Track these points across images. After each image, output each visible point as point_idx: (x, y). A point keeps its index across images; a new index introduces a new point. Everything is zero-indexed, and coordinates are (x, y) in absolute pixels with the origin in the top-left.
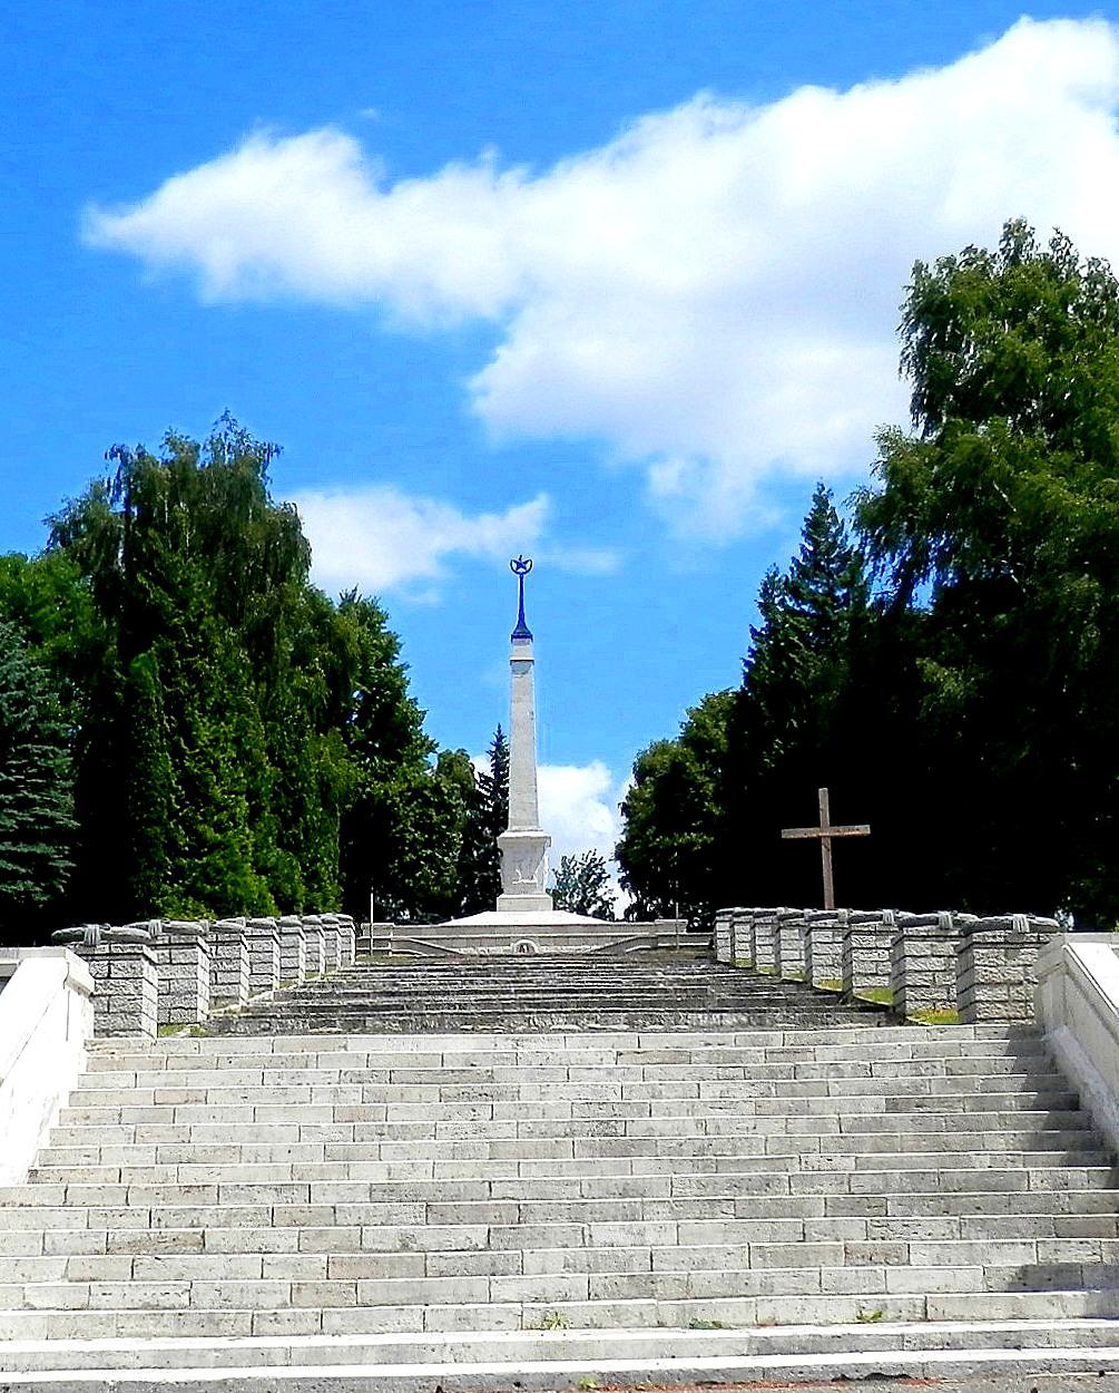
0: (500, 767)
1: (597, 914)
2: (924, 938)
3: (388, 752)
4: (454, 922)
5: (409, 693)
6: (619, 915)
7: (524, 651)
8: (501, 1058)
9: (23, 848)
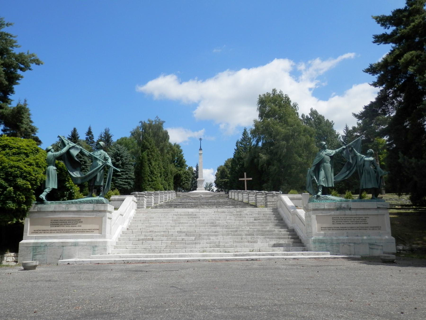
0: (197, 167)
1: (211, 191)
2: (260, 195)
4: (190, 192)
5: (184, 158)
6: (215, 191)
7: (201, 152)
8: (197, 212)
9: (126, 181)
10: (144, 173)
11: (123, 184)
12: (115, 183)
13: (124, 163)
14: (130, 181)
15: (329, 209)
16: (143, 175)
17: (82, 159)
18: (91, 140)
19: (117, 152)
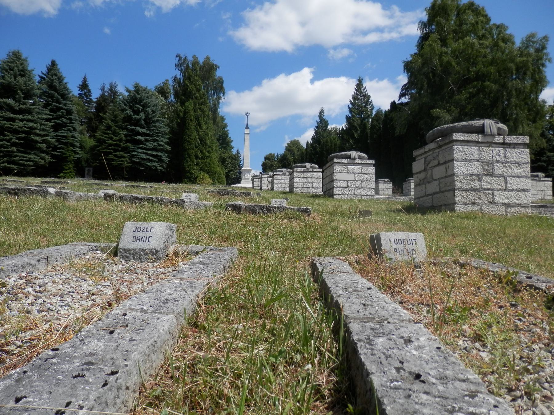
3: (225, 148)
5: (229, 136)
7: (247, 131)
9: (155, 153)
10: (189, 142)
11: (149, 159)
12: (131, 157)
13: (150, 119)
14: (162, 154)
17: (61, 106)
18: (87, 97)
19: (135, 95)
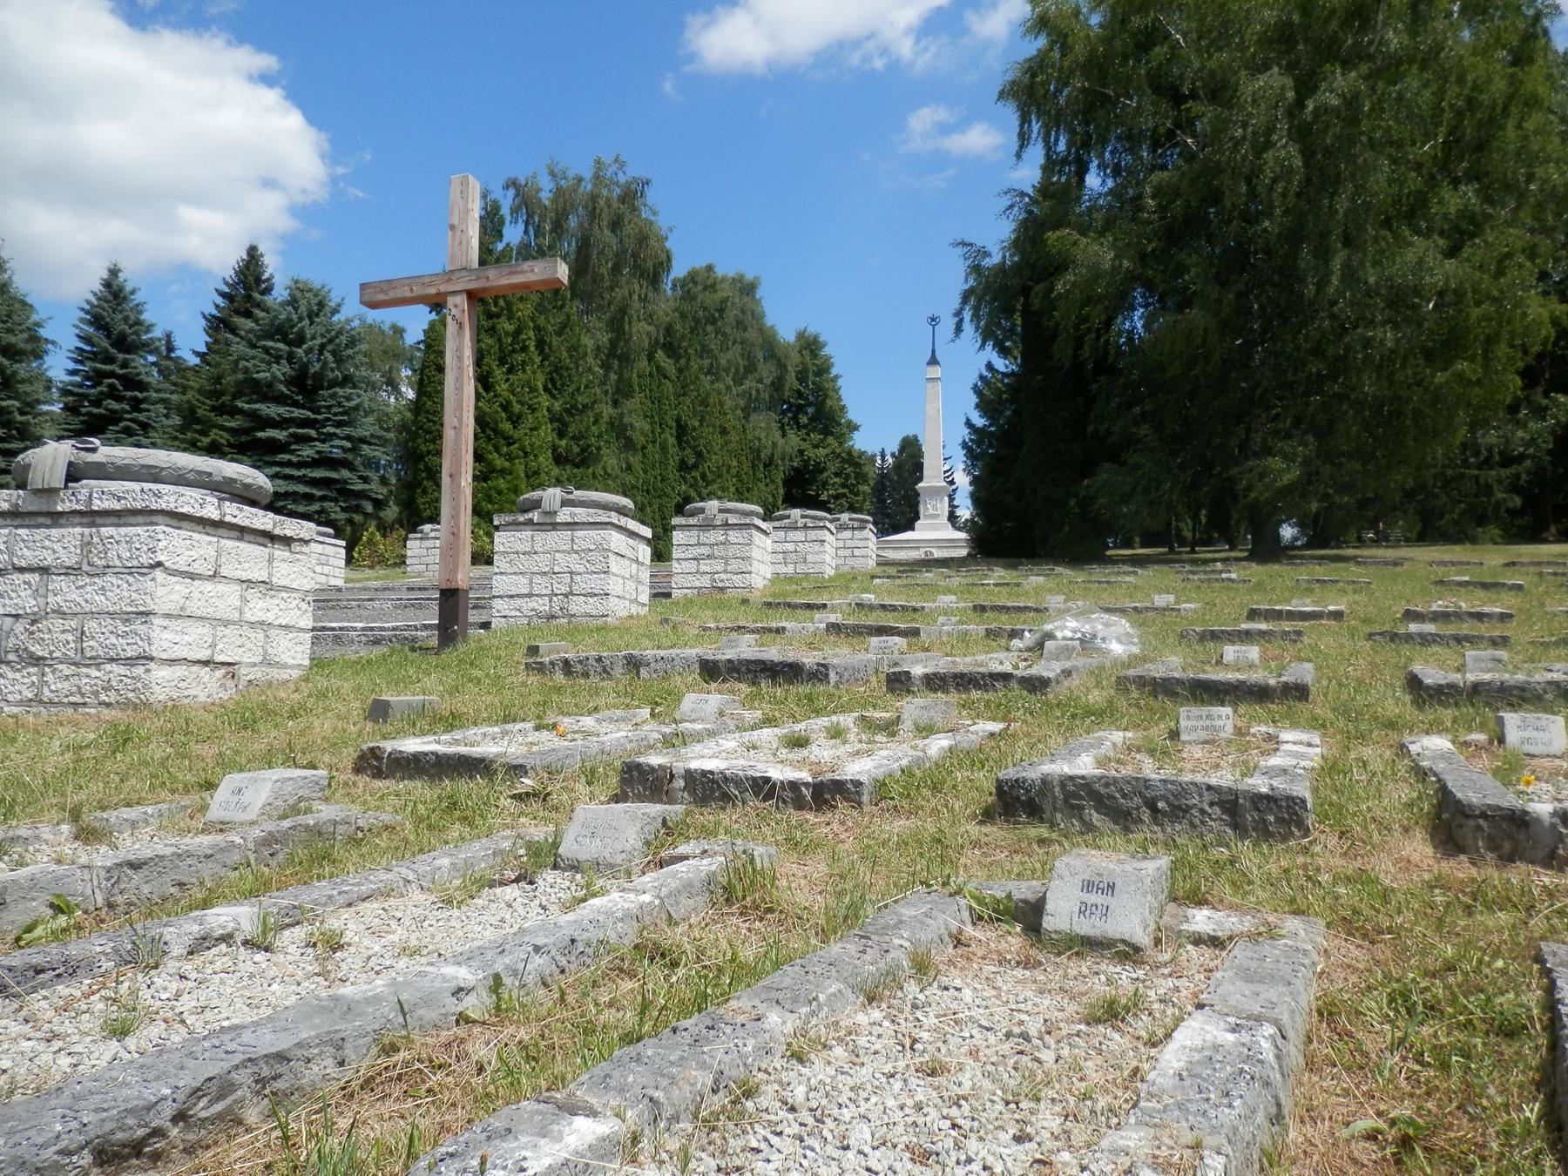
7: (936, 372)
9: (319, 473)
10: (428, 432)
11: (295, 493)
15: (156, 479)
16: (426, 441)
